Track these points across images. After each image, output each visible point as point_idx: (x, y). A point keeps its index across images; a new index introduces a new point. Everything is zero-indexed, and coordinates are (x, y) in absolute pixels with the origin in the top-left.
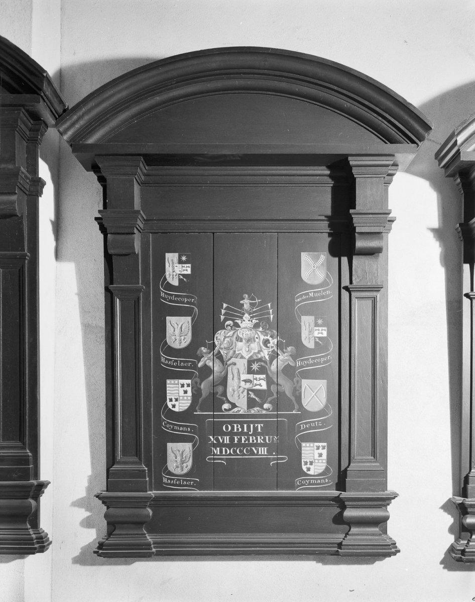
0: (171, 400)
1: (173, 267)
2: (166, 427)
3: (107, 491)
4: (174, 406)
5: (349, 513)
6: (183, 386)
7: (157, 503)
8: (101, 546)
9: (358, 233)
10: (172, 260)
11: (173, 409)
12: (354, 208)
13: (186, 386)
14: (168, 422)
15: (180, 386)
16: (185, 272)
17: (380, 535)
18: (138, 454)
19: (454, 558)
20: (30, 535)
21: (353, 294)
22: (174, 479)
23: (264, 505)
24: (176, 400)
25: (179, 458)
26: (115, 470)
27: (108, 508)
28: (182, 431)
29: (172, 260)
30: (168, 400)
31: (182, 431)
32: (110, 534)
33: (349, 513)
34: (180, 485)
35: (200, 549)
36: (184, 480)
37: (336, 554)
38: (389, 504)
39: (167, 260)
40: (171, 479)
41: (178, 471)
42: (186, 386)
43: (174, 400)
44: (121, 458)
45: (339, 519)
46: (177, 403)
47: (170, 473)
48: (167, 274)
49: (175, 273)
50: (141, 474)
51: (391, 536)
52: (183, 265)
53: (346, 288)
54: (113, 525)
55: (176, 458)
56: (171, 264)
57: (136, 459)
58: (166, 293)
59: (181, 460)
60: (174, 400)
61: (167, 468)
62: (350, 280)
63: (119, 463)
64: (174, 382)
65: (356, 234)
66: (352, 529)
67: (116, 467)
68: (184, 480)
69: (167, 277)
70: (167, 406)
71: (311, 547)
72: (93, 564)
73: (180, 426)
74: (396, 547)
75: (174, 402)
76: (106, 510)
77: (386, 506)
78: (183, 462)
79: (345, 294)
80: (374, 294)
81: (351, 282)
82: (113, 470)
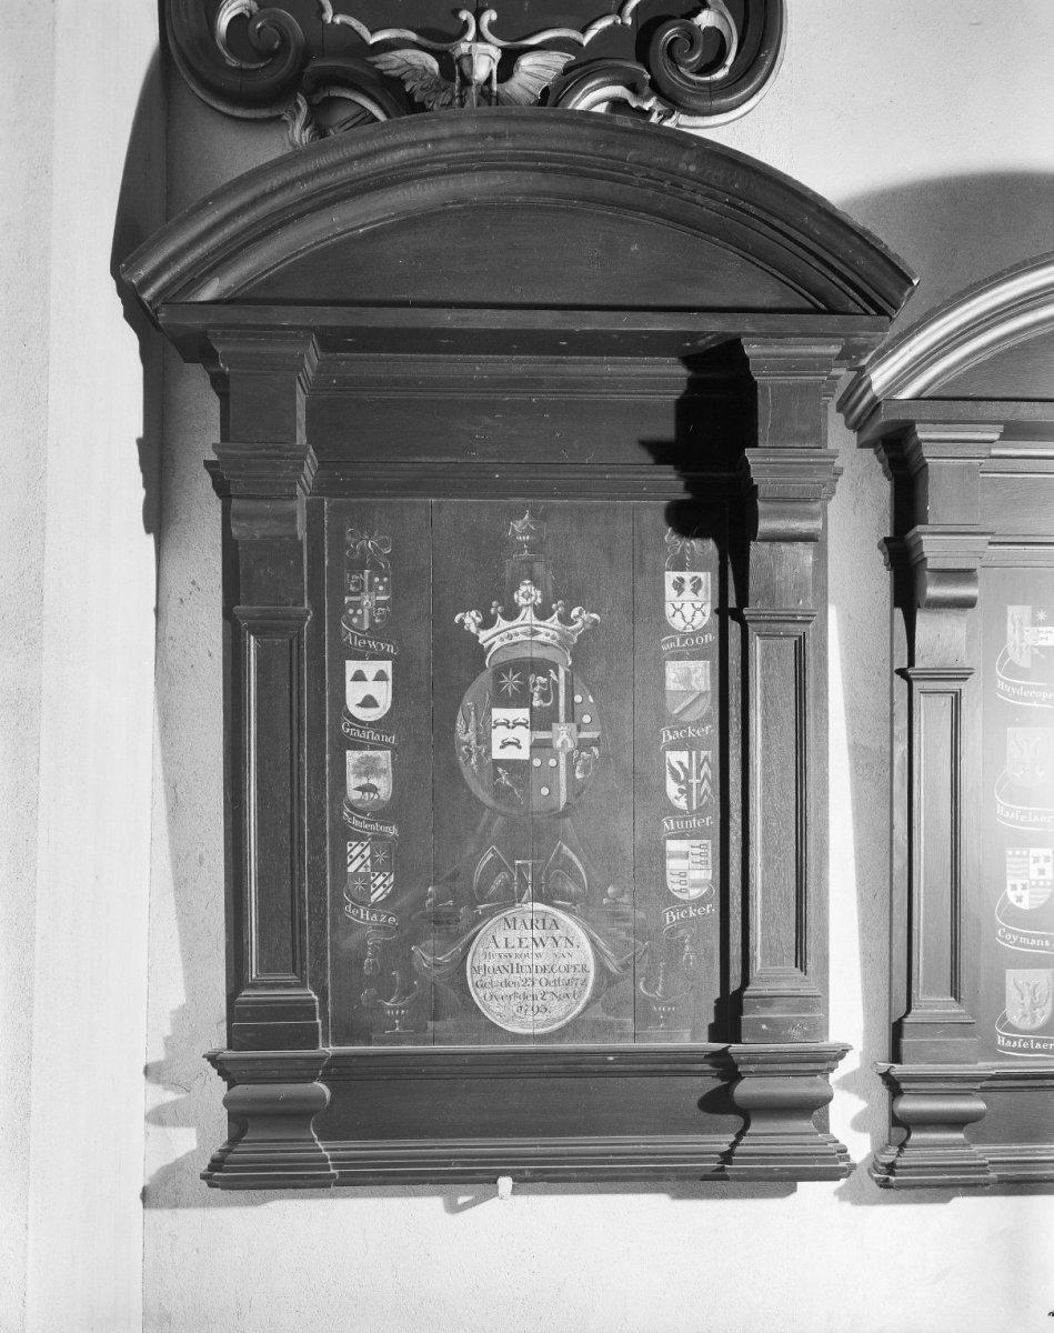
0: (1014, 887)
1: (1021, 631)
2: (1004, 940)
3: (230, 1047)
4: (1019, 899)
5: (746, 1089)
6: (1036, 860)
7: (336, 1071)
8: (216, 1164)
9: (932, 570)
10: (1020, 620)
11: (1018, 904)
12: (926, 523)
13: (1042, 859)
14: (1008, 931)
15: (1032, 860)
16: (1040, 643)
17: (816, 1134)
18: (296, 966)
19: (877, 1180)
20: (320, 1150)
21: (916, 685)
22: (1017, 1039)
23: (536, 1075)
24: (1024, 887)
25: (1027, 999)
26: (247, 1002)
27: (229, 1088)
28: (1034, 947)
29: (1020, 620)
30: (1009, 887)
31: (1034, 947)
32: (234, 1139)
33: (746, 1089)
34: (1029, 1051)
35: (909, 1178)
36: (1036, 1041)
37: (719, 1177)
38: (832, 1070)
39: (1009, 618)
40: (1012, 1039)
41: (1027, 1024)
42: (1042, 859)
43: (1019, 887)
44: (257, 975)
45: (719, 1103)
46: (1026, 894)
47: (1011, 1028)
48: (1010, 644)
49: (1024, 644)
50: (306, 1009)
51: (837, 1138)
52: (1040, 629)
53: (902, 673)
54: (241, 1119)
55: (1022, 998)
56: (1017, 626)
57: (291, 978)
58: (1007, 683)
59: (1032, 1001)
60: (1019, 887)
61: (1004, 1018)
62: (742, 647)
63: (254, 986)
64: (1014, 853)
65: (927, 573)
66: (752, 1125)
67: (247, 994)
68: (1036, 1041)
69: (1010, 651)
70: (1006, 897)
71: (685, 1161)
72: (205, 1204)
73: (1030, 937)
74: (848, 1157)
75: (1019, 892)
76: (225, 1092)
77: (826, 1073)
78: (1034, 1006)
79: (901, 684)
80: (954, 686)
81: (911, 662)
82: (241, 1003)
